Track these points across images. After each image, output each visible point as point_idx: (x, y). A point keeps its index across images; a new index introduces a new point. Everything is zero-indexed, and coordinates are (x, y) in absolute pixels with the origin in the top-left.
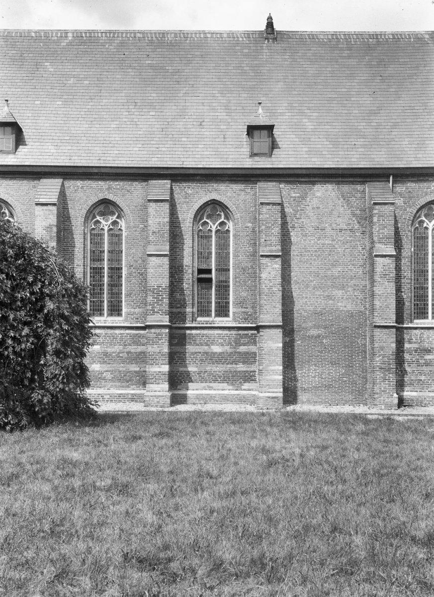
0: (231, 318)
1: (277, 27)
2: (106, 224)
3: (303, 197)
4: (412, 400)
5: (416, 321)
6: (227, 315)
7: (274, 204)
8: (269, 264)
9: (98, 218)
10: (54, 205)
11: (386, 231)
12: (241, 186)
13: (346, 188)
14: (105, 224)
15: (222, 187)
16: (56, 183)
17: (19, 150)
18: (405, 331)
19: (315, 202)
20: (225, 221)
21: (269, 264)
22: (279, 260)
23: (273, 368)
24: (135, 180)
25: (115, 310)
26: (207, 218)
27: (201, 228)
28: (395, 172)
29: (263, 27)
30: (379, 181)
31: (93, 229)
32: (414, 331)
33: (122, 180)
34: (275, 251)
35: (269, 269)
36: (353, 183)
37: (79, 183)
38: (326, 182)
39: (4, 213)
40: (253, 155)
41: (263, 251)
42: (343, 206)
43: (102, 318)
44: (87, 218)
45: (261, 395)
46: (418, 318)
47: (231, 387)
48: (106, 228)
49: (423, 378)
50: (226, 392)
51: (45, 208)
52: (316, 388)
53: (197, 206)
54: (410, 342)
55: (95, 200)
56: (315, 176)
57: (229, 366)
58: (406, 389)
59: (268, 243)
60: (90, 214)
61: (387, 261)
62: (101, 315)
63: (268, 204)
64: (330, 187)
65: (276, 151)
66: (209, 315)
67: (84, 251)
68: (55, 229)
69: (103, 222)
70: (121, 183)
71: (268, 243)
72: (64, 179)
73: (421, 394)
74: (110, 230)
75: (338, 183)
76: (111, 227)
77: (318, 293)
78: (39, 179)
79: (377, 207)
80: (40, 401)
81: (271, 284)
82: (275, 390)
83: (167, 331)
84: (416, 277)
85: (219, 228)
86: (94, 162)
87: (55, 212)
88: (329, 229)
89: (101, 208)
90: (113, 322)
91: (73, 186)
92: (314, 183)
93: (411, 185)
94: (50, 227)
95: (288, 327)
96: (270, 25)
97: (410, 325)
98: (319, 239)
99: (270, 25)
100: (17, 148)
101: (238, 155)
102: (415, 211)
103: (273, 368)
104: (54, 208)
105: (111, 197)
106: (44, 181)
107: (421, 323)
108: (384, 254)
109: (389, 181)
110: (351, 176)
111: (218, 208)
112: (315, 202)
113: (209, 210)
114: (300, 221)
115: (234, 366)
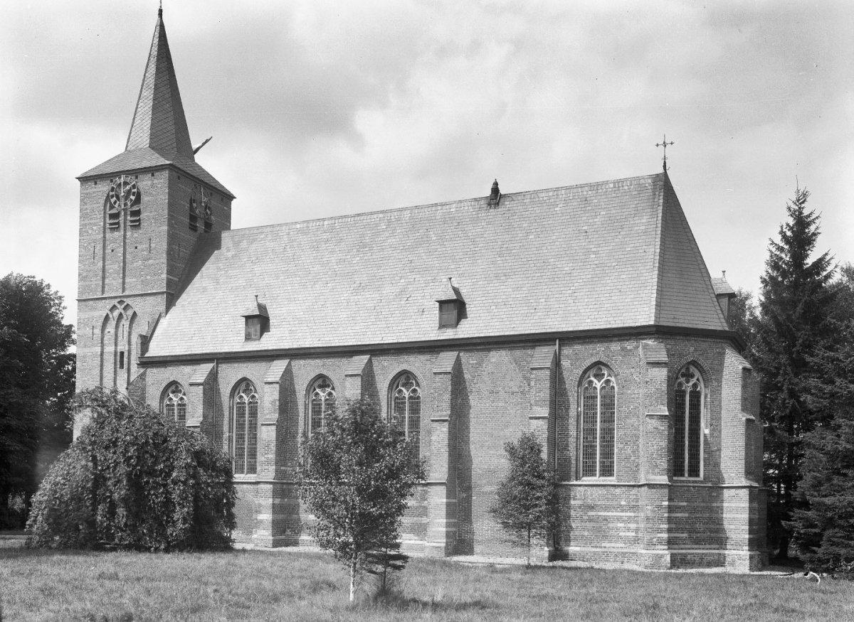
0: (614, 478)
1: (502, 191)
2: (696, 378)
3: (480, 364)
4: (575, 555)
5: (585, 478)
6: (612, 475)
7: (445, 373)
8: (438, 428)
9: (317, 390)
10: (277, 383)
11: (542, 394)
12: (428, 357)
13: (518, 353)
14: (323, 395)
15: (412, 358)
16: (365, 358)
17: (264, 336)
18: (572, 488)
19: (490, 368)
20: (417, 388)
21: (438, 428)
22: (446, 424)
23: (438, 521)
24: (343, 357)
25: (253, 469)
26: (403, 386)
27: (397, 395)
28: (559, 336)
29: (488, 193)
30: (547, 345)
31: (314, 400)
32: (579, 488)
33: (333, 357)
34: (445, 416)
35: (438, 432)
36: (524, 348)
37: (302, 362)
38: (500, 348)
39: (251, 389)
40: (442, 326)
41: (434, 416)
42: (515, 370)
43: (242, 475)
44: (308, 391)
45: (427, 544)
46: (586, 476)
47: (416, 538)
48: (323, 399)
49: (586, 533)
50: (412, 542)
51: (271, 386)
52: (489, 541)
53: (391, 377)
54: (574, 499)
55: (313, 375)
56: (489, 343)
57: (415, 518)
58: (572, 543)
59: (440, 408)
60: (310, 388)
61: (540, 422)
62: (242, 472)
63: (440, 373)
64: (503, 353)
65: (463, 322)
66: (683, 475)
67: (305, 418)
68: (277, 403)
69: (321, 394)
70: (333, 360)
71: (440, 408)
72: (460, 351)
73: (583, 549)
74: (326, 400)
75: (511, 349)
76: (327, 397)
77: (492, 452)
78: (351, 357)
79: (534, 372)
80: (171, 535)
81: (439, 446)
82: (439, 540)
83: (271, 486)
84: (585, 436)
85: (411, 394)
86: (404, 339)
87: (278, 389)
88: (502, 393)
89: (320, 382)
90: (604, 481)
91: (298, 365)
92: (489, 350)
93: (578, 347)
94: (274, 401)
95: (258, 483)
96: (495, 190)
97: (575, 483)
98: (493, 402)
99: (495, 190)
100: (261, 335)
101: (428, 328)
102: (581, 373)
103: (438, 521)
104: (277, 386)
105: (325, 373)
106: (356, 358)
107: (589, 481)
108: (537, 416)
109: (555, 344)
110: (521, 341)
111: (602, 367)
112: (490, 368)
113: (403, 380)
114: (477, 386)
115: (420, 519)
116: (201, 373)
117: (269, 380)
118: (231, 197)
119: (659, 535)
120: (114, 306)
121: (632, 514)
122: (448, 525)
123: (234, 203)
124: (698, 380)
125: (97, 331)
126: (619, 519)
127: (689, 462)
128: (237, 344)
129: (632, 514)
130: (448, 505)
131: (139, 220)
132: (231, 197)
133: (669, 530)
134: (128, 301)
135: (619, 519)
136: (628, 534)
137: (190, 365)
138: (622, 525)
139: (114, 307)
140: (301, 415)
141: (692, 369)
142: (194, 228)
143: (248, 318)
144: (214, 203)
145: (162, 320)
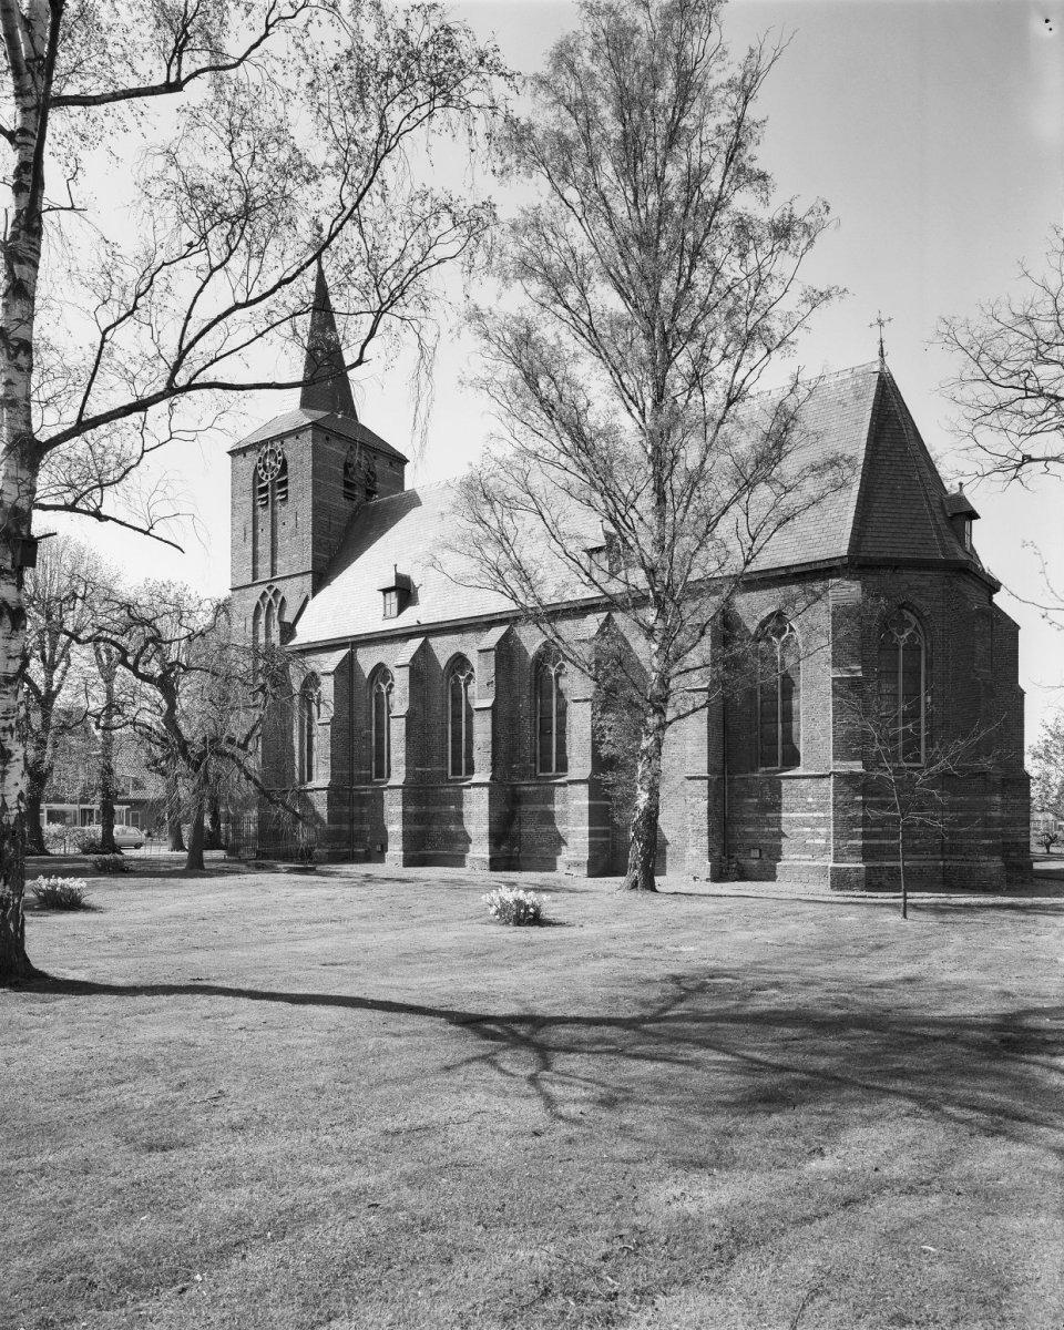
78: (407, 641)
91: (435, 642)
116: (332, 660)
117: (400, 663)
118: (402, 461)
119: (850, 842)
120: (264, 593)
121: (822, 815)
122: (591, 834)
123: (408, 468)
124: (916, 628)
125: (250, 621)
126: (805, 823)
127: (898, 656)
128: (376, 623)
129: (822, 815)
130: (591, 808)
131: (286, 492)
132: (402, 461)
133: (864, 836)
134: (277, 585)
135: (805, 823)
136: (817, 841)
137: (780, 585)
138: (808, 829)
139: (264, 594)
140: (297, 747)
141: (907, 614)
142: (350, 497)
143: (385, 591)
144: (380, 466)
145: (310, 603)
